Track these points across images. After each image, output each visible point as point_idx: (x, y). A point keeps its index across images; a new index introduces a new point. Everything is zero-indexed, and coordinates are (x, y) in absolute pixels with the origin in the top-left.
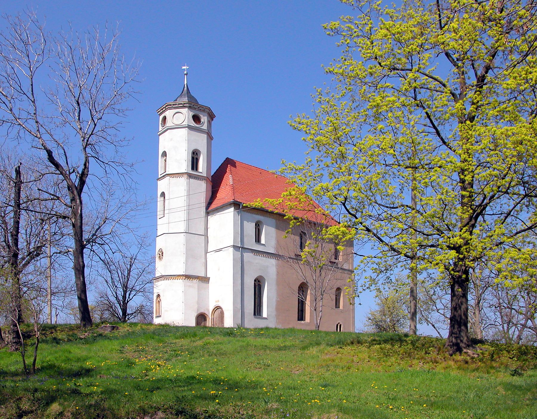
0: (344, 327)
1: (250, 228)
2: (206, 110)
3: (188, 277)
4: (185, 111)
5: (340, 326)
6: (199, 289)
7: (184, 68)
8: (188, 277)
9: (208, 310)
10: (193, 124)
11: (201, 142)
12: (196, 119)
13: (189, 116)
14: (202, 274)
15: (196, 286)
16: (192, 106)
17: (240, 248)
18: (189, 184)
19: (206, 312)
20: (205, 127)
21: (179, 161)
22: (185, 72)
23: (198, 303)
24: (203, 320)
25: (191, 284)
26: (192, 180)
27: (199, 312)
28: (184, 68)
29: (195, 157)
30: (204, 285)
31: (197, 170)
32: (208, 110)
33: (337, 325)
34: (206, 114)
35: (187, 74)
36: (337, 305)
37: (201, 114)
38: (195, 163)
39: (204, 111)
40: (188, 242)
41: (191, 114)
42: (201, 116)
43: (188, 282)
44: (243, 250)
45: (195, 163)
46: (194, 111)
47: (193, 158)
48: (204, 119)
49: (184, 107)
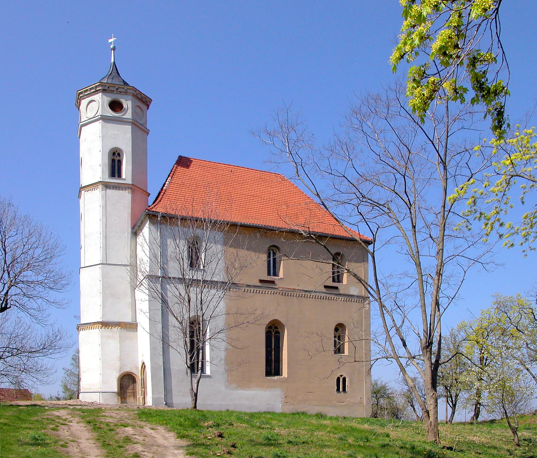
0: (351, 383)
1: (178, 248)
2: (129, 91)
3: (105, 324)
4: (98, 97)
5: (344, 379)
6: (121, 340)
7: (110, 41)
8: (105, 324)
9: (137, 368)
10: (110, 113)
11: (123, 137)
12: (116, 106)
13: (103, 103)
14: (128, 319)
15: (117, 335)
16: (106, 88)
17: (160, 280)
18: (105, 198)
19: (134, 371)
20: (129, 115)
21: (92, 166)
22: (112, 46)
23: (121, 359)
24: (131, 382)
25: (111, 334)
26: (110, 192)
27: (123, 371)
28: (110, 41)
29: (117, 158)
30: (130, 334)
31: (120, 176)
32: (132, 91)
33: (338, 379)
34: (130, 97)
35: (114, 49)
36: (339, 350)
37: (123, 96)
38: (117, 168)
39: (126, 93)
40: (105, 277)
41: (107, 99)
42: (123, 101)
43: (107, 332)
44: (164, 280)
45: (117, 168)
46: (110, 95)
47: (113, 161)
48: (127, 103)
49: (96, 92)
